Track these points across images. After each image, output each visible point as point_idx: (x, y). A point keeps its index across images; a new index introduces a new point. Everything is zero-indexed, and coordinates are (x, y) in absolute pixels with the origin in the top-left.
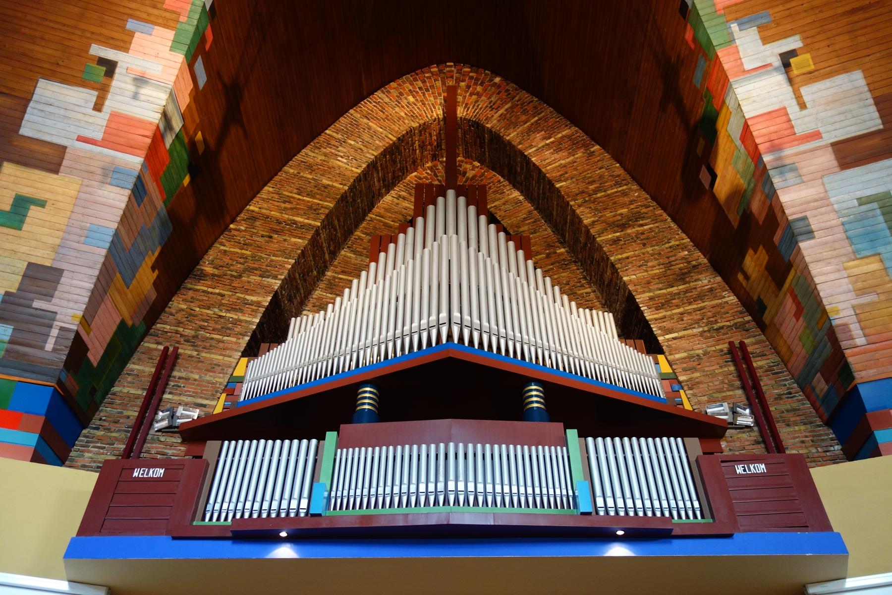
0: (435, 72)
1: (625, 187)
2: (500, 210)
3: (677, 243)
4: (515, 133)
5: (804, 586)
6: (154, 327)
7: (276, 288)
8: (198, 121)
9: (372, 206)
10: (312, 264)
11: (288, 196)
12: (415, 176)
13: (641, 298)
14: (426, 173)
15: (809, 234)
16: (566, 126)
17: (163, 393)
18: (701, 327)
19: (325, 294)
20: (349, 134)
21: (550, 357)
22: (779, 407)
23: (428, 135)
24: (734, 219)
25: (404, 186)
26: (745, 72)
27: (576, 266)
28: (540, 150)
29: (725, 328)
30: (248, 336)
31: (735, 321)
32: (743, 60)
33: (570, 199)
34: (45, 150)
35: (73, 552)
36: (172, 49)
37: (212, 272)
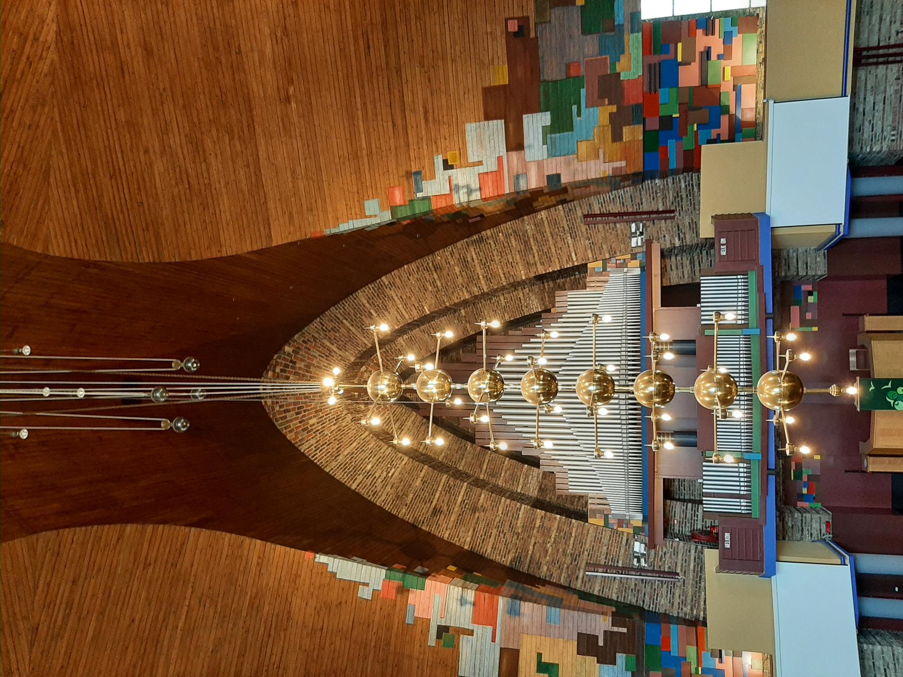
30: (571, 521)
34: (505, 661)
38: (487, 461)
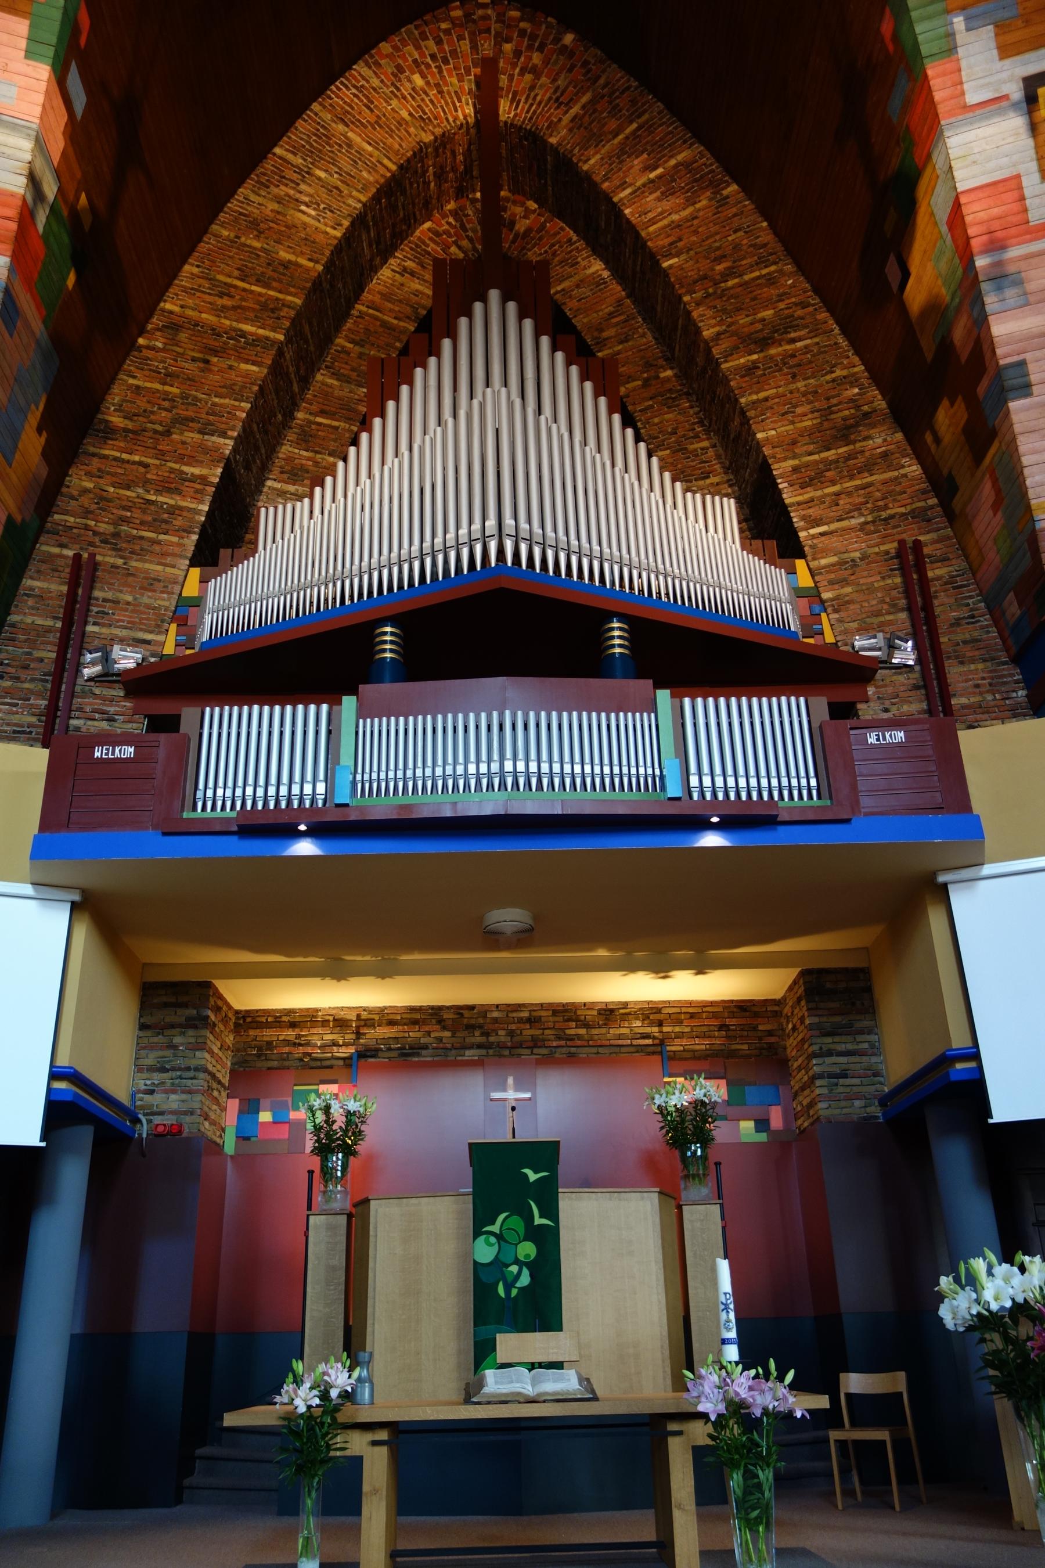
0: (457, 18)
1: (773, 268)
2: (570, 297)
3: (845, 373)
4: (598, 156)
5: (935, 874)
6: (50, 519)
7: (227, 452)
8: (79, 175)
9: (360, 289)
10: (276, 405)
11: (225, 284)
12: (429, 230)
13: (779, 469)
14: (449, 223)
15: (1025, 389)
16: (685, 142)
17: (86, 623)
18: (863, 515)
19: (297, 451)
20: (315, 155)
21: (640, 576)
22: (953, 637)
23: (448, 154)
24: (928, 347)
25: (411, 249)
26: (967, 108)
27: (689, 401)
28: (639, 193)
29: (897, 517)
30: (195, 533)
31: (914, 506)
32: (966, 86)
33: (683, 290)
35: (38, 852)
36: (29, 54)
37: (122, 425)
38: (335, 423)
